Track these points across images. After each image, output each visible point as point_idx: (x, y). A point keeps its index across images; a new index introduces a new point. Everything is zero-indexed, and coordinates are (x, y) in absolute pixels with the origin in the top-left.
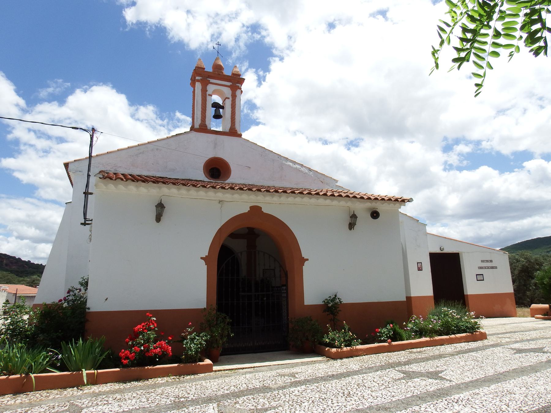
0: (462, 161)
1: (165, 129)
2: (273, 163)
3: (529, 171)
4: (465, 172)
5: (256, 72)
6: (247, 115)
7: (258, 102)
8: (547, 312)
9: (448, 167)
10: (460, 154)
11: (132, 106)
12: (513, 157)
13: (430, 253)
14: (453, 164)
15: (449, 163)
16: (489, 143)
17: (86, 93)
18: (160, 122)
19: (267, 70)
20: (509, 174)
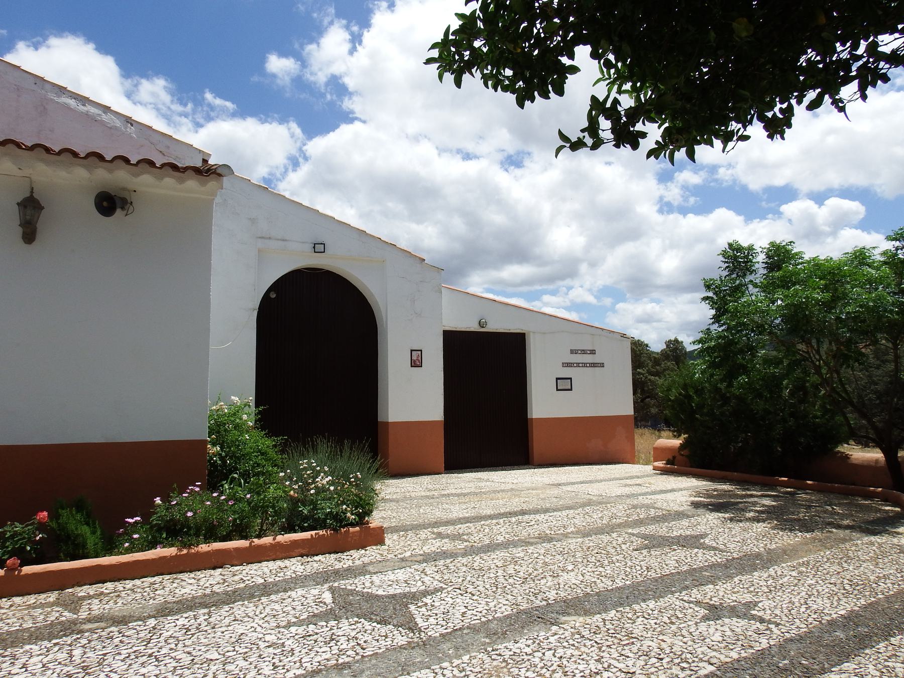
0: (687, 198)
1: (188, 121)
2: (19, 96)
3: (790, 221)
4: (691, 216)
5: (347, 27)
6: (332, 104)
7: (350, 82)
8: (674, 457)
9: (665, 207)
10: (685, 188)
11: (127, 79)
12: (766, 195)
13: (446, 333)
14: (672, 202)
15: (666, 200)
16: (730, 172)
17: (38, 51)
18: (177, 108)
19: (366, 24)
20: (759, 222)
